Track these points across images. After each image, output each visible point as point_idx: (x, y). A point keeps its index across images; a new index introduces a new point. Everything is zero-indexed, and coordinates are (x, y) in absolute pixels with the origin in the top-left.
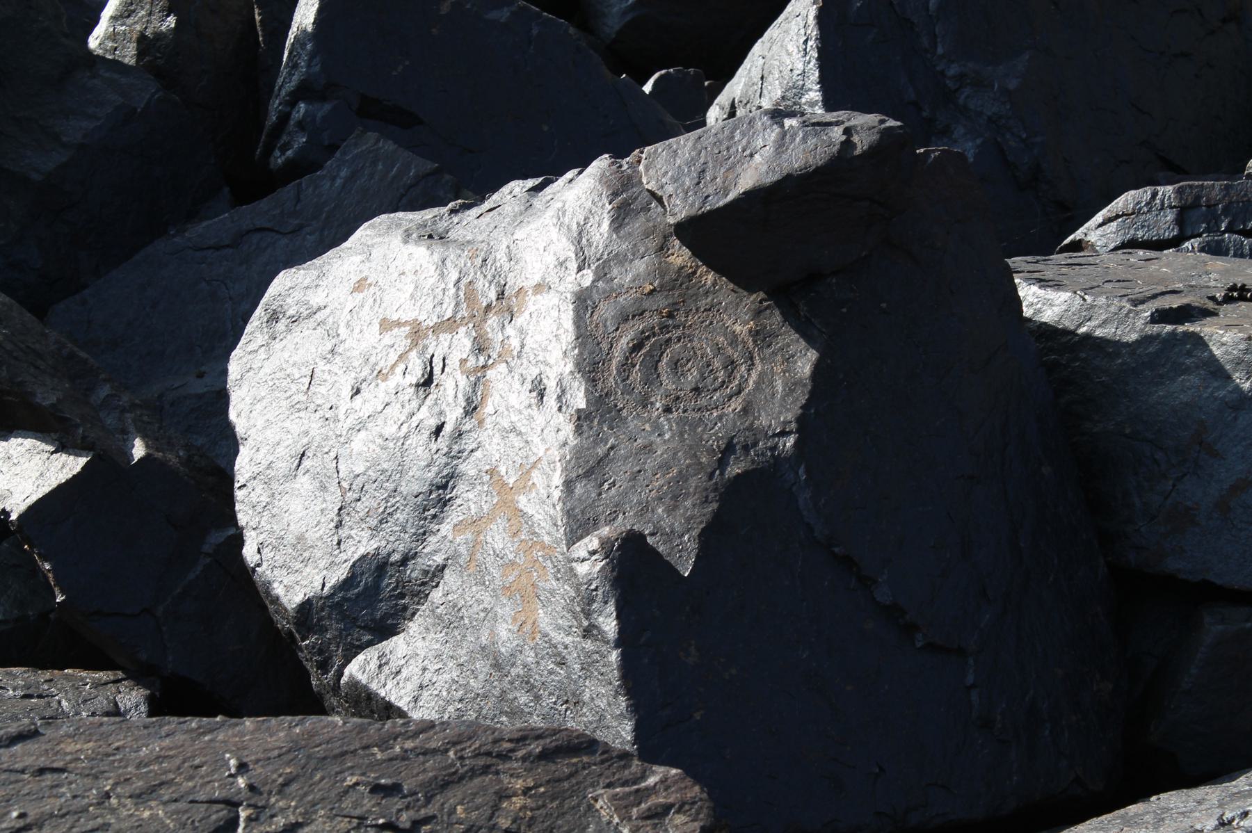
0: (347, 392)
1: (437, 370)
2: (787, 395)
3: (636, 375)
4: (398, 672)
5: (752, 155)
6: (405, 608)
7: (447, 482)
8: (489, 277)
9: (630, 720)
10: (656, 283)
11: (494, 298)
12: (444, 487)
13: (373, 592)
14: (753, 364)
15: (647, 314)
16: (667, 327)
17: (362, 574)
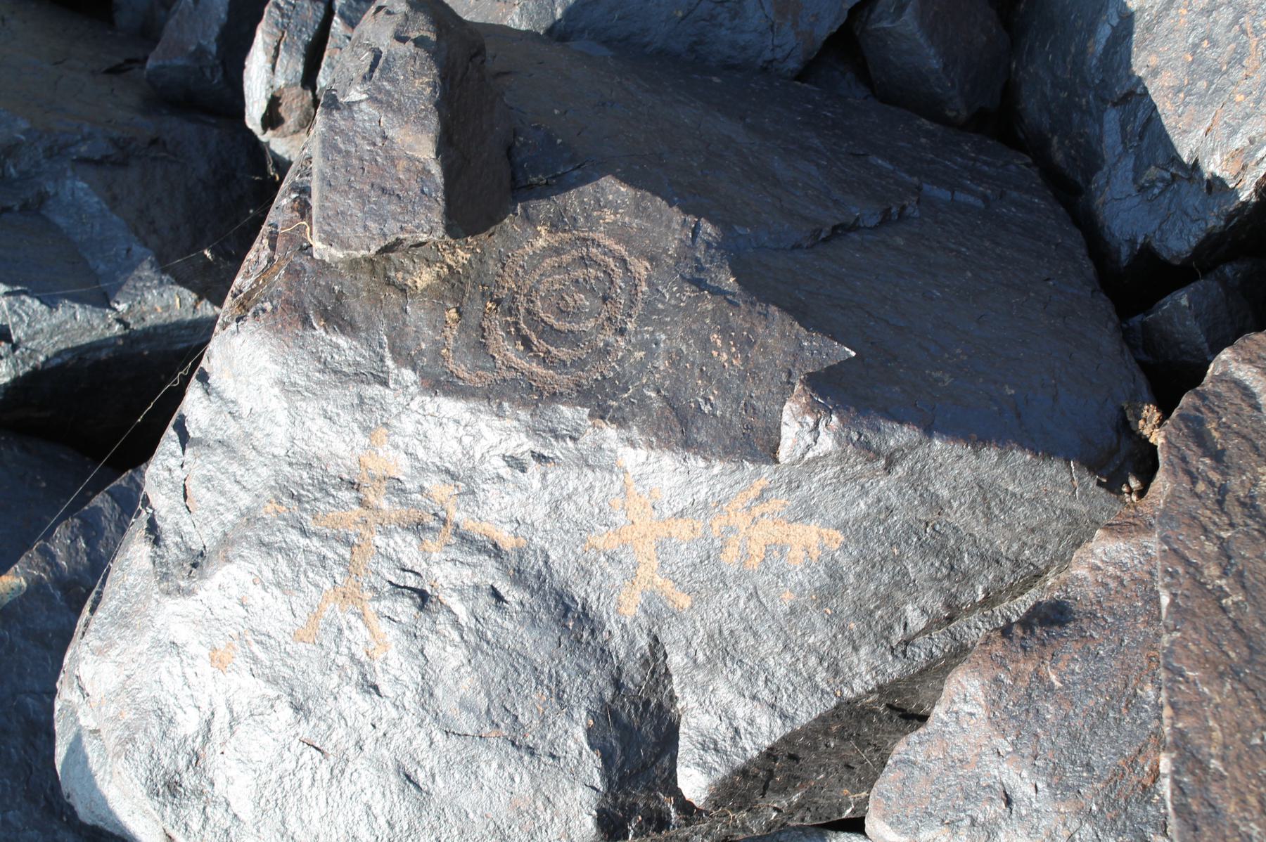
0: (363, 703)
1: (411, 581)
2: (648, 217)
3: (563, 353)
4: (736, 731)
5: (385, 138)
6: (660, 705)
7: (563, 603)
8: (318, 495)
9: (1011, 449)
10: (449, 305)
11: (354, 494)
12: (567, 609)
13: (627, 733)
14: (593, 240)
15: (485, 324)
16: (510, 309)
17: (604, 738)
